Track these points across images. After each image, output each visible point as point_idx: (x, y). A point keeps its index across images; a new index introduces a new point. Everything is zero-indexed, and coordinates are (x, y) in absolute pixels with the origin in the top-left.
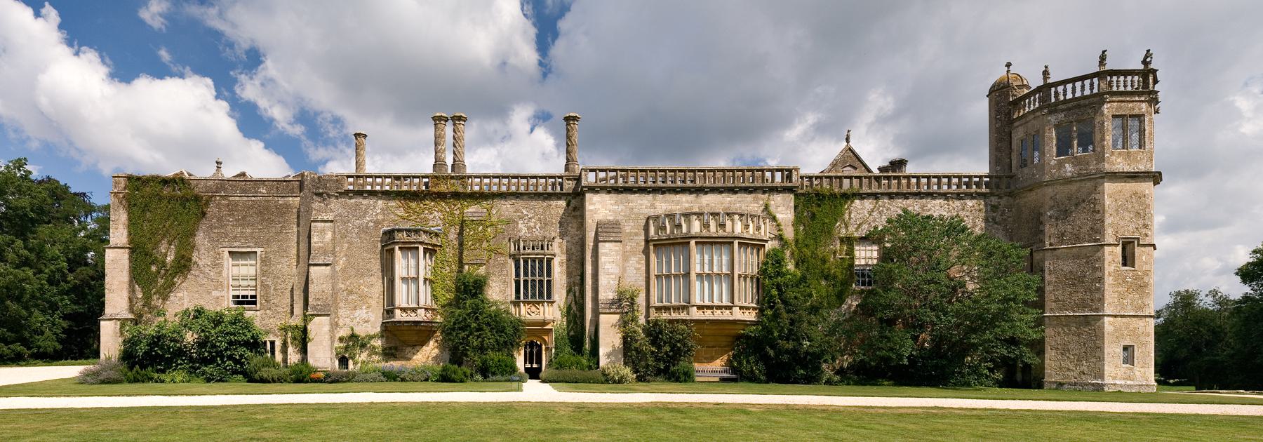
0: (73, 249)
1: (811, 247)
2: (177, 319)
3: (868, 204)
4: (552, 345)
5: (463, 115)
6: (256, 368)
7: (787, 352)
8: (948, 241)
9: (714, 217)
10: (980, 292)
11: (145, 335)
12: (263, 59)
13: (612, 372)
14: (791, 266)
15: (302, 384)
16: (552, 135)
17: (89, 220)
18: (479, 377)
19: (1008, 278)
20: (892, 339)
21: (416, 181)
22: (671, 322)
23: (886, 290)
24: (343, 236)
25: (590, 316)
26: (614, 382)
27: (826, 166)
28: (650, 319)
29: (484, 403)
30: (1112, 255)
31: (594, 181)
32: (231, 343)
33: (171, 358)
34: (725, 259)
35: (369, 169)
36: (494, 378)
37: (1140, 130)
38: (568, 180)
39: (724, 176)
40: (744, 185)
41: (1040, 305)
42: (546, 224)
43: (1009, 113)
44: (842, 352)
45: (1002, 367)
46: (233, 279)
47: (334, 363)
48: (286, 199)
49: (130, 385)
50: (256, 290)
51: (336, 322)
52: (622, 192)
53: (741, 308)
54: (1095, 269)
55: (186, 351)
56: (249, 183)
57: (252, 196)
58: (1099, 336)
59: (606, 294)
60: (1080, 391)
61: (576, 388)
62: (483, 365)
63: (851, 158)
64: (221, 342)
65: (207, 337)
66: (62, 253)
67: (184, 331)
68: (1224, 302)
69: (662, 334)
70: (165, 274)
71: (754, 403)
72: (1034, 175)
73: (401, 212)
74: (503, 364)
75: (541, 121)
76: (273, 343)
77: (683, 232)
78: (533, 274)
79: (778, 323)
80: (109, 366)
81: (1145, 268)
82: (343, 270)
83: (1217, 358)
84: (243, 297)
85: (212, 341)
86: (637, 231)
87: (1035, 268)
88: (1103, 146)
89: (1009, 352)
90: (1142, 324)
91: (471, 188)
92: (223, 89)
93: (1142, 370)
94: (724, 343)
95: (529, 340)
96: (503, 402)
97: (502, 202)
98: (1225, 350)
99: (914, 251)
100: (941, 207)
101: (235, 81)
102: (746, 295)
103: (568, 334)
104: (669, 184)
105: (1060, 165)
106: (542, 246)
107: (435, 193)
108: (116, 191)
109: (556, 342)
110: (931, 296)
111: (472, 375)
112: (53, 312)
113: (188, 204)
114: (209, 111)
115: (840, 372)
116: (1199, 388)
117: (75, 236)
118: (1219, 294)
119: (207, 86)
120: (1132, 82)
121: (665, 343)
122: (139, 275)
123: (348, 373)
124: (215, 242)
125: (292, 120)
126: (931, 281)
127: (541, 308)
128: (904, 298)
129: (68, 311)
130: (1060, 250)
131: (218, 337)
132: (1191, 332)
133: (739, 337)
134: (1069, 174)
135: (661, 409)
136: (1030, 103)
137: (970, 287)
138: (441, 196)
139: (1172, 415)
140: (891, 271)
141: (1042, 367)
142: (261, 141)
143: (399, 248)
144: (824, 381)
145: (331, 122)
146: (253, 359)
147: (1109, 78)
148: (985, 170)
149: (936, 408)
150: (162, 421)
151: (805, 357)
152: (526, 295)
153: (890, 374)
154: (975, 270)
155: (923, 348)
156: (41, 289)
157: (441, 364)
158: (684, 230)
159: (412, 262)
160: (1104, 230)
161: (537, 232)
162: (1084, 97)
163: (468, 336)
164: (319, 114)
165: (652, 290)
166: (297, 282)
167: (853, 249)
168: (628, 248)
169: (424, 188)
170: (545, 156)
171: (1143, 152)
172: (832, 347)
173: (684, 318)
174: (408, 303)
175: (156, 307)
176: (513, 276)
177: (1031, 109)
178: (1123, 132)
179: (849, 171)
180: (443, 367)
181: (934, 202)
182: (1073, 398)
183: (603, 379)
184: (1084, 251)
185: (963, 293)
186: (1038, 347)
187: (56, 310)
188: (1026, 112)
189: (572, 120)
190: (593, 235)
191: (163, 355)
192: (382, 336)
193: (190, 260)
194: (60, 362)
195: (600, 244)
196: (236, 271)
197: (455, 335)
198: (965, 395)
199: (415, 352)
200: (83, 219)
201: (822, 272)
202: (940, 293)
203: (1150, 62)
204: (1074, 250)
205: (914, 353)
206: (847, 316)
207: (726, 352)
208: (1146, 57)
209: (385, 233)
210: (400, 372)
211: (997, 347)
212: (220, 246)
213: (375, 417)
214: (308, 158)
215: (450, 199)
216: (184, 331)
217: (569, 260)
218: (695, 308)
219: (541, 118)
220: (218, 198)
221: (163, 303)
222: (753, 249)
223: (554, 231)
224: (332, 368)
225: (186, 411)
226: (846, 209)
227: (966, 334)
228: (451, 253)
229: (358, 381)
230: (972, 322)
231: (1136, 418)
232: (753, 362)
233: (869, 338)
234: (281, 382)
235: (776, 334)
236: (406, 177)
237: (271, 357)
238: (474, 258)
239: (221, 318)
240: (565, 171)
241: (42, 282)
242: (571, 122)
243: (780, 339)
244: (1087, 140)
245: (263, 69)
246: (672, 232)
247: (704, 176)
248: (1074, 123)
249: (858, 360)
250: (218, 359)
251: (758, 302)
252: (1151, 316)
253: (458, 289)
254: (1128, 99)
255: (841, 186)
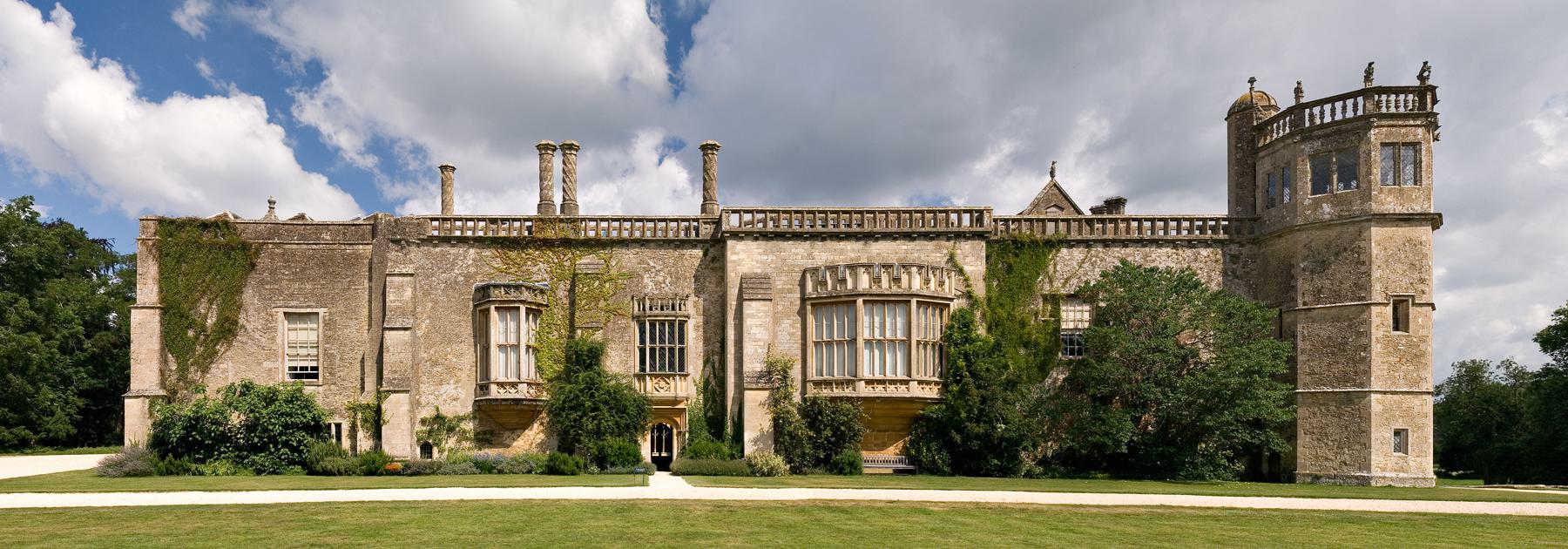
0: (91, 309)
1: (1007, 307)
2: (219, 396)
3: (1078, 253)
4: (685, 428)
5: (575, 143)
6: (318, 457)
7: (977, 437)
8: (1177, 299)
9: (886, 269)
10: (1216, 363)
11: (180, 417)
12: (327, 73)
13: (759, 462)
14: (981, 331)
15: (375, 477)
16: (685, 167)
17: (110, 273)
18: (594, 468)
19: (1252, 346)
20: (1107, 421)
21: (517, 224)
22: (833, 399)
23: (1100, 360)
24: (426, 293)
25: (733, 392)
26: (763, 474)
27: (1026, 206)
28: (806, 396)
29: (601, 500)
30: (1381, 317)
31: (738, 225)
32: (286, 426)
33: (213, 445)
34: (900, 321)
35: (458, 209)
36: (613, 469)
37: (1415, 161)
38: (705, 223)
39: (899, 219)
40: (923, 229)
41: (1291, 378)
42: (678, 279)
43: (1253, 141)
44: (1045, 438)
45: (1244, 456)
46: (289, 347)
47: (414, 451)
48: (356, 247)
49: (162, 478)
50: (318, 360)
51: (418, 400)
52: (772, 239)
53: (920, 382)
54: (1360, 334)
55: (231, 436)
56: (309, 227)
57: (313, 244)
58: (1364, 417)
59: (753, 365)
60: (1340, 485)
61: (715, 482)
62: (600, 453)
63: (1057, 196)
64: (274, 424)
65: (257, 419)
66: (77, 314)
67: (229, 411)
68: (1519, 375)
69: (821, 415)
70: (205, 340)
71: (936, 500)
72: (1283, 217)
73: (498, 263)
74: (625, 453)
75: (672, 150)
76: (338, 426)
77: (848, 288)
78: (662, 341)
79: (966, 401)
80: (135, 455)
81: (1422, 332)
82: (426, 336)
83: (1511, 445)
84: (302, 368)
85: (263, 423)
86: (791, 287)
87: (1284, 332)
88: (1370, 182)
89: (1252, 438)
90: (1418, 403)
91: (585, 234)
92: (277, 110)
93: (1418, 459)
94: (899, 426)
95: (656, 422)
96: (624, 500)
97: (624, 251)
98: (1521, 435)
99: (1135, 312)
100: (1169, 257)
101: (292, 100)
102: (926, 366)
103: (705, 415)
104: (830, 228)
105: (1317, 205)
106: (673, 306)
107: (540, 240)
108: (144, 237)
109: (690, 425)
110: (1156, 368)
111: (586, 466)
112: (66, 387)
113: (233, 253)
114: (259, 138)
115: (1043, 462)
116: (1489, 482)
117: (94, 293)
118: (1514, 366)
119: (256, 107)
120: (1406, 101)
121: (826, 426)
122: (172, 341)
123: (433, 464)
124: (267, 301)
125: (363, 149)
126: (1156, 350)
127: (672, 383)
128: (1123, 370)
129: (84, 386)
130: (1316, 311)
131: (270, 418)
132: (1479, 412)
133: (917, 419)
134: (1328, 217)
135: (820, 508)
136: (1278, 128)
137: (1205, 356)
138: (547, 244)
139: (1455, 515)
140: (1106, 336)
141: (1293, 456)
142: (324, 175)
143: (496, 307)
144: (1023, 474)
145: (411, 152)
146: (314, 446)
147: (1376, 97)
148: (1223, 211)
149: (1162, 506)
150: (202, 522)
151: (1000, 444)
152: (653, 366)
153: (1105, 464)
154: (1211, 336)
155: (1146, 432)
156: (50, 359)
157: (548, 452)
158: (850, 285)
159: (512, 325)
160: (1371, 286)
161: (666, 289)
162: (1345, 121)
163: (581, 417)
164: (396, 142)
165: (809, 360)
166: (369, 350)
167: (1059, 309)
168: (780, 308)
169: (526, 233)
170: (676, 194)
171: (1419, 189)
172: (1033, 430)
173: (850, 395)
174: (506, 376)
175: (194, 382)
176: (637, 343)
177: (1281, 135)
178: (1395, 164)
179: (1053, 213)
180: (550, 456)
181: (1159, 251)
182: (1332, 494)
183: (749, 471)
184: (1345, 312)
185: (1196, 364)
186: (1289, 431)
187: (70, 385)
188: (1274, 139)
189: (710, 149)
190: (737, 291)
191: (203, 441)
192: (475, 418)
193: (235, 323)
194: (75, 449)
195: (745, 303)
196: (293, 336)
197: (565, 416)
198: (1198, 491)
199: (515, 437)
200: (102, 272)
201: (1021, 338)
202: (1167, 363)
203: (1428, 77)
204: (1333, 310)
205: (1135, 439)
206: (1052, 393)
207: (902, 437)
208: (1423, 71)
209: (478, 290)
210: (497, 462)
211: (1237, 431)
212: (273, 305)
213: (466, 518)
214: (382, 196)
215: (558, 247)
216: (229, 411)
217: (706, 323)
218: (863, 382)
219: (672, 147)
220: (270, 246)
221: (203, 377)
222: (934, 309)
223: (688, 287)
224: (412, 458)
225: (231, 510)
226: (1051, 260)
227: (1199, 414)
228: (560, 315)
229: (445, 474)
230: (1207, 400)
231: (1410, 519)
232: (935, 450)
233: (1079, 420)
234: (349, 475)
235: (963, 415)
236: (504, 220)
237: (337, 443)
238: (588, 320)
239: (274, 395)
240: (702, 213)
241: (53, 350)
242: (709, 152)
243: (968, 421)
244: (1350, 174)
245: (327, 85)
246: (834, 288)
247: (875, 218)
248: (1334, 153)
249: (1065, 447)
250: (271, 446)
251: (941, 376)
252: (1429, 393)
253: (568, 359)
254: (1400, 123)
255: (1044, 232)
